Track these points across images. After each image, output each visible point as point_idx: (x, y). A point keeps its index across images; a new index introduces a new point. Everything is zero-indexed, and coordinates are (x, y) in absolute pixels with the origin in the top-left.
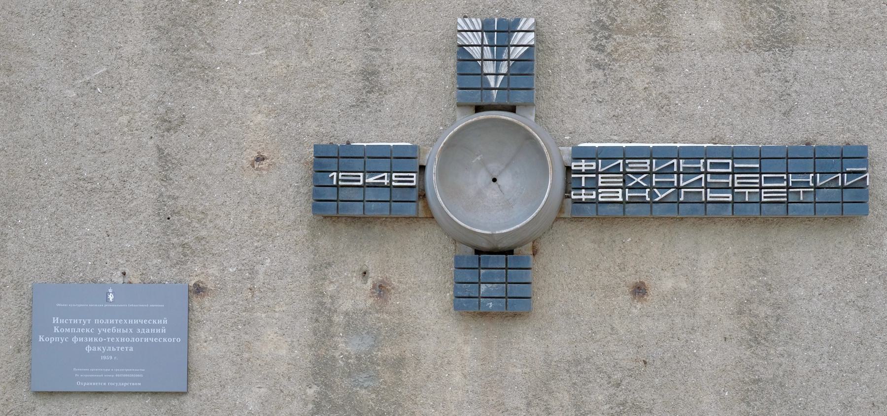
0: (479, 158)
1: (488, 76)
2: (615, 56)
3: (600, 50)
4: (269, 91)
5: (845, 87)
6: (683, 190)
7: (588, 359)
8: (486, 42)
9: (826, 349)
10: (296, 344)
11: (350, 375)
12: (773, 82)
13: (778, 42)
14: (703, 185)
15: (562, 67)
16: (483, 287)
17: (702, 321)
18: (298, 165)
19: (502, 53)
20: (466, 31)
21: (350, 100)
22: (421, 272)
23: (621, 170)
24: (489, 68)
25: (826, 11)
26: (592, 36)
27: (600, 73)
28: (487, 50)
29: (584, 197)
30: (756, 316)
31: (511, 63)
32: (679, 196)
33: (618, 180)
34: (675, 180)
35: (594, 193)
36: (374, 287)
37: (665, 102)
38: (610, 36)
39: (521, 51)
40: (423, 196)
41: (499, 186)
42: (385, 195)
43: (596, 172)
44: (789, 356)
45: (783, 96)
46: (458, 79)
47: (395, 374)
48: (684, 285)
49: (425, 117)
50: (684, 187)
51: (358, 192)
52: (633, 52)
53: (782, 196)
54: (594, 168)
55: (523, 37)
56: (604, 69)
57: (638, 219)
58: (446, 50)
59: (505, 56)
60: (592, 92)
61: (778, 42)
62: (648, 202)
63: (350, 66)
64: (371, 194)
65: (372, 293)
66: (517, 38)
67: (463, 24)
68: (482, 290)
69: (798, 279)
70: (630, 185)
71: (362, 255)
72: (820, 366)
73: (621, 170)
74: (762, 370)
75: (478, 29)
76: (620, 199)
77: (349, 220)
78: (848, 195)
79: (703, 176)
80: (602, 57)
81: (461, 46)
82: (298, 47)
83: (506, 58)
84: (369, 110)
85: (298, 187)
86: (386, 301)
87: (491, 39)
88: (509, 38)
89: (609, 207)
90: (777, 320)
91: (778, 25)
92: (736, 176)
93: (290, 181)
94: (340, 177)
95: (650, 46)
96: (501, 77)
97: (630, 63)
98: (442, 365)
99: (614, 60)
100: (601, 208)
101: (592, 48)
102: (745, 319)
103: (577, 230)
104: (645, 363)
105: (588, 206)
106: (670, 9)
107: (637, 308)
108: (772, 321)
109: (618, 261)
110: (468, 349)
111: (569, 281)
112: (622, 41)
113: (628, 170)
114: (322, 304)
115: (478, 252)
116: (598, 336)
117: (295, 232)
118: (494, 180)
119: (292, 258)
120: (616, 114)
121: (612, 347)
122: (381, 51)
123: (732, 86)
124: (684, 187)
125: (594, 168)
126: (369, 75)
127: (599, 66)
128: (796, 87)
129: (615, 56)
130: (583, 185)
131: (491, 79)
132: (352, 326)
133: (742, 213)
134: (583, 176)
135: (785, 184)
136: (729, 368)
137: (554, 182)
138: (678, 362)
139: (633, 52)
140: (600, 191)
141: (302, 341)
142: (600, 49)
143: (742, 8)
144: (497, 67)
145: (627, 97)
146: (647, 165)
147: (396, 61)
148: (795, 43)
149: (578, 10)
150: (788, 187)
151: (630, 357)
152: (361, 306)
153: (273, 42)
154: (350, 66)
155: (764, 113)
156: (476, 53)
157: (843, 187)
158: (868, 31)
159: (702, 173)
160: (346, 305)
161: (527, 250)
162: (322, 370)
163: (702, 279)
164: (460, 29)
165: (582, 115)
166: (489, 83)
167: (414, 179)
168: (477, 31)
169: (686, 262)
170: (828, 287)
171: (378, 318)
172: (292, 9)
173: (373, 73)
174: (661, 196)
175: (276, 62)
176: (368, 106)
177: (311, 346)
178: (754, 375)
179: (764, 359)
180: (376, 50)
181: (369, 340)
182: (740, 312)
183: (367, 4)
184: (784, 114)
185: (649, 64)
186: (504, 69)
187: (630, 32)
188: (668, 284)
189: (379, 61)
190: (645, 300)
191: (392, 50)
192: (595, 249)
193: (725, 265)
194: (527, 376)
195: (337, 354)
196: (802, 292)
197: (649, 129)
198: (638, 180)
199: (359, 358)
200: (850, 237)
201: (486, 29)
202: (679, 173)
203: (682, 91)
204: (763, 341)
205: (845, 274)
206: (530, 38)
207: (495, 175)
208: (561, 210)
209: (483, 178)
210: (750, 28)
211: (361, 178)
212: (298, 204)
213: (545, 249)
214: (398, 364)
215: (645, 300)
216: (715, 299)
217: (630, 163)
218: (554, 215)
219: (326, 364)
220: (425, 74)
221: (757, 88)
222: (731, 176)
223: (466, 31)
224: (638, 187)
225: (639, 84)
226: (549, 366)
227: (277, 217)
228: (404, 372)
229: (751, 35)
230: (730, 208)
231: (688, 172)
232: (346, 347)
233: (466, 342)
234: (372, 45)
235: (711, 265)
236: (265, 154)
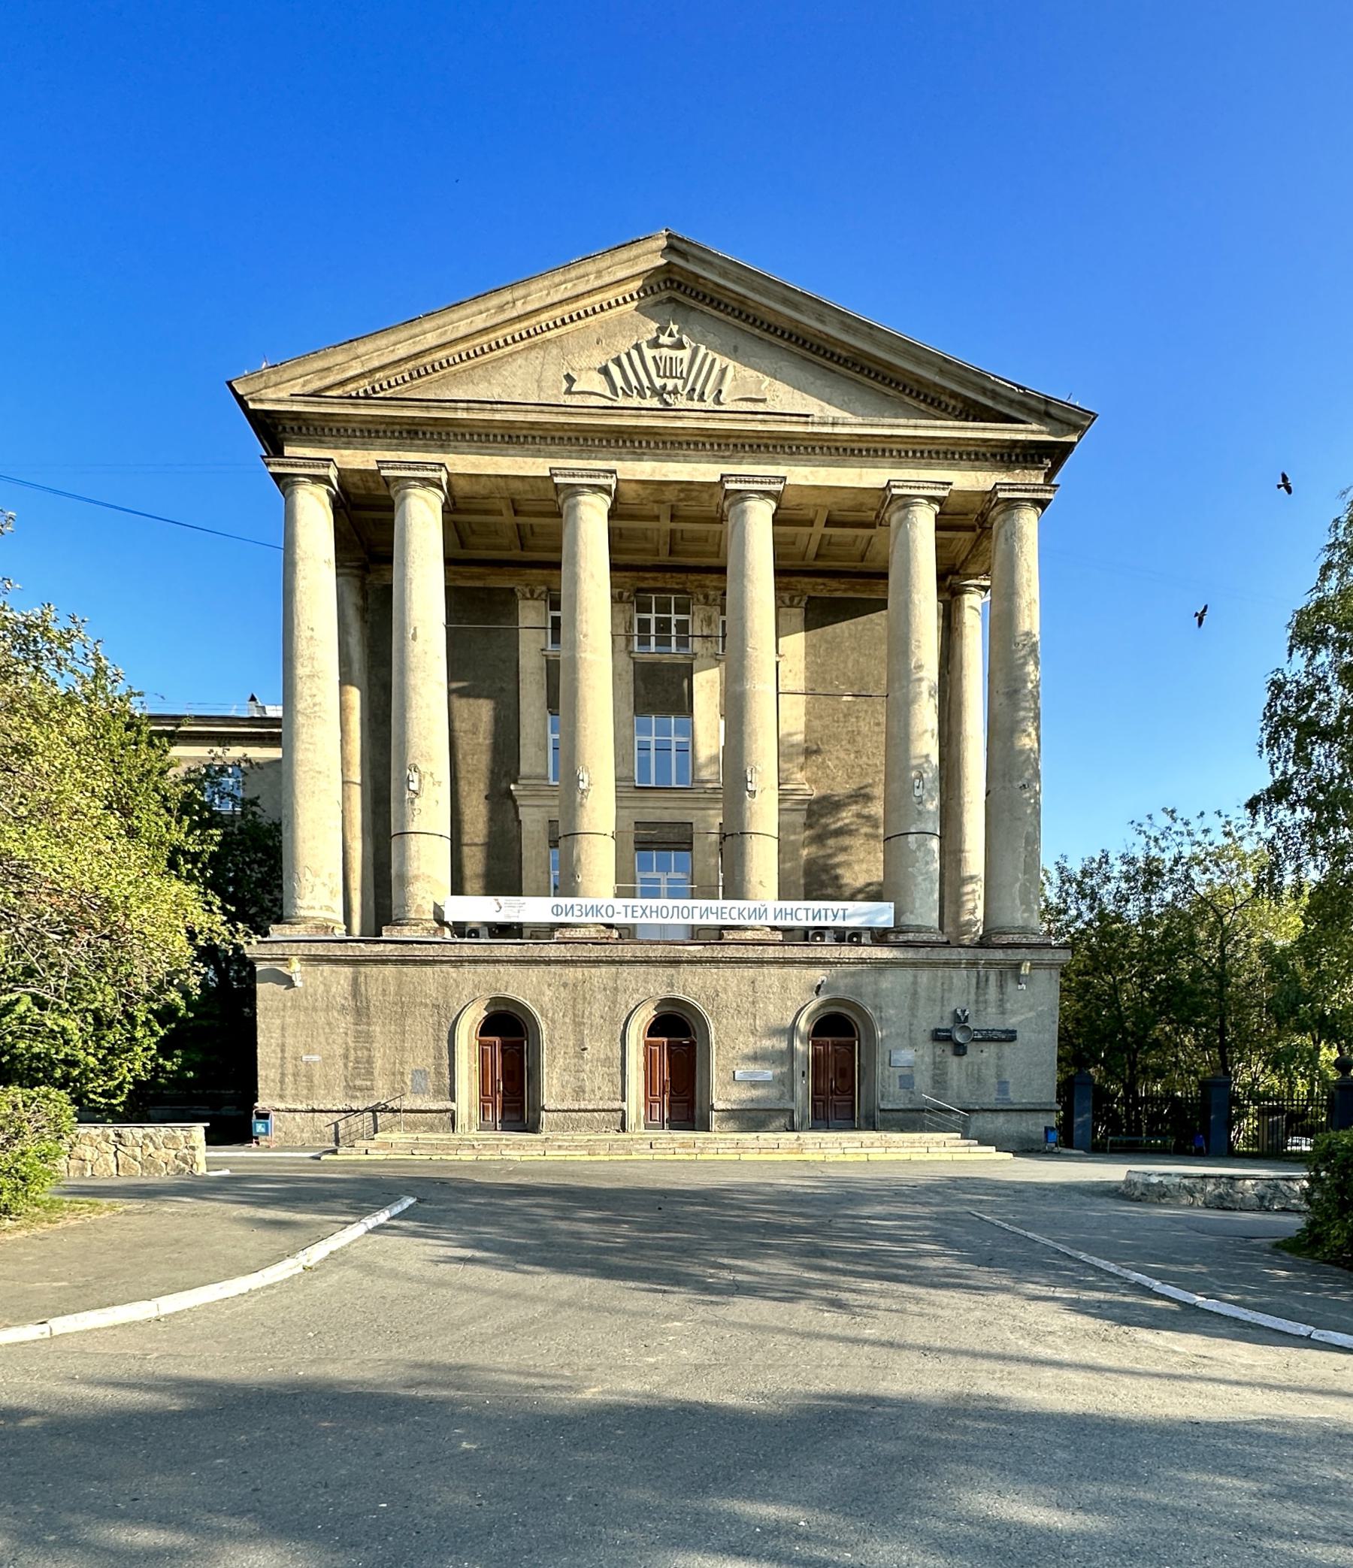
22: (949, 1049)
51: (939, 1037)
93: (927, 1035)
133: (999, 1040)
162: (934, 1063)
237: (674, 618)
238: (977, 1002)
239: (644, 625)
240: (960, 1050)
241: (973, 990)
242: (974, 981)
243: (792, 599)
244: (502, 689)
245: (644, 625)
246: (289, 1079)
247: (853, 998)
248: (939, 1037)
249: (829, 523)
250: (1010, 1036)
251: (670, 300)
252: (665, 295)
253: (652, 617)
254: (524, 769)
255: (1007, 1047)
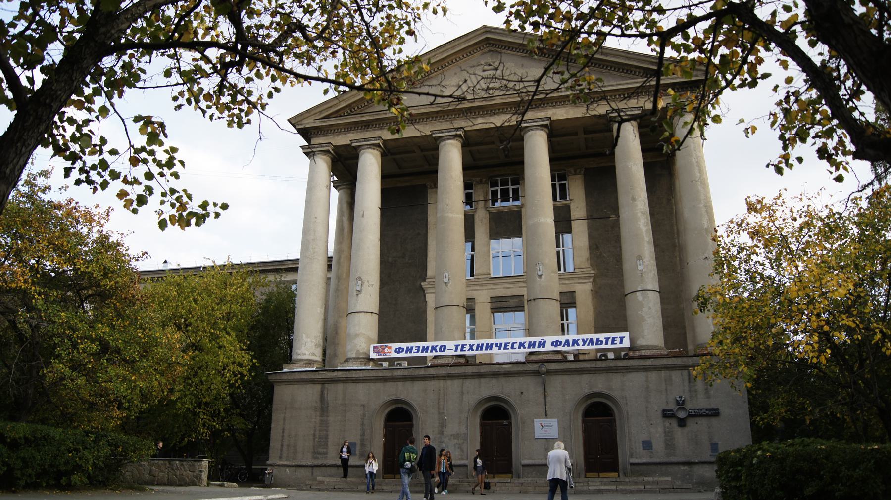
13: (709, 397)
22: (674, 423)
51: (667, 415)
93: (659, 413)
162: (665, 432)
237: (511, 188)
238: (690, 391)
239: (495, 193)
240: (682, 423)
241: (686, 383)
242: (686, 377)
243: (575, 171)
244: (419, 234)
245: (495, 193)
246: (285, 448)
247: (607, 392)
248: (667, 415)
249: (585, 132)
250: (715, 413)
251: (490, 51)
252: (487, 50)
253: (499, 189)
254: (430, 273)
255: (714, 421)
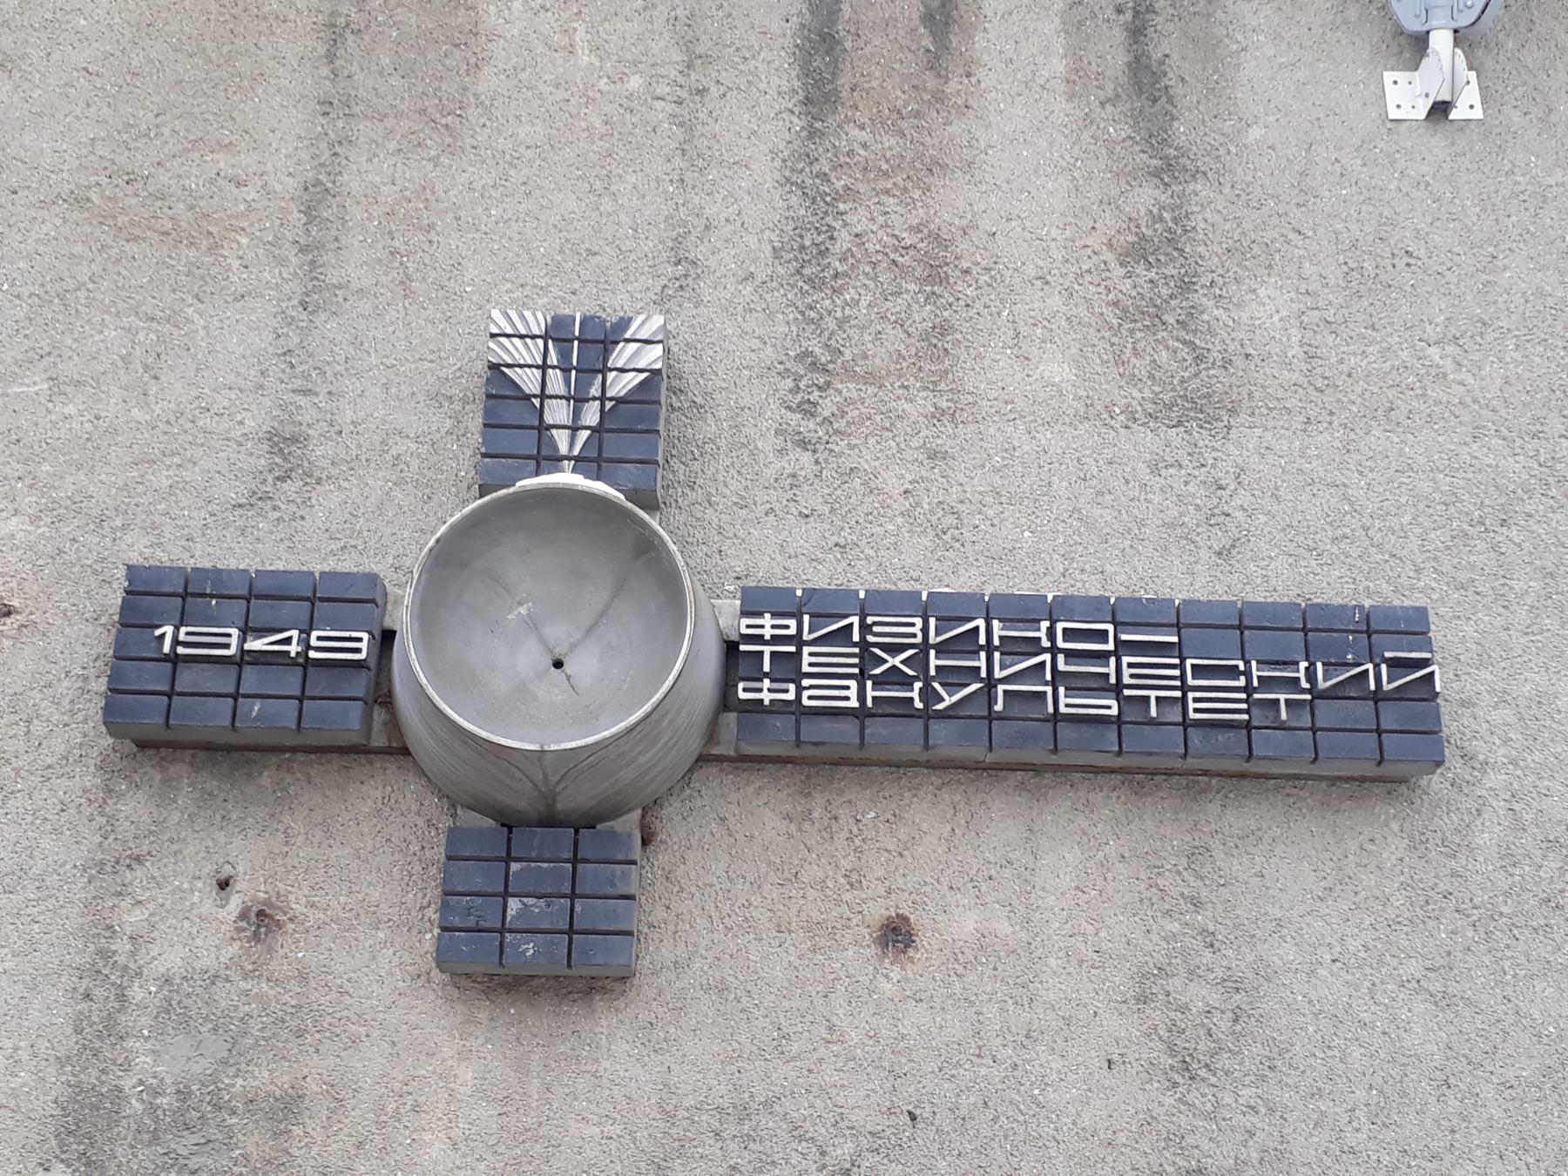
0: (523, 610)
1: (554, 432)
2: (840, 424)
3: (806, 412)
4: (46, 467)
5: (1351, 504)
6: (1001, 688)
7: (767, 1104)
8: (553, 359)
9: (1360, 1094)
10: (24, 1055)
11: (155, 1138)
12: (1190, 488)
13: (1196, 408)
14: (1048, 677)
15: (722, 443)
16: (514, 905)
17: (1051, 1016)
18: (90, 629)
19: (590, 384)
20: (508, 336)
21: (233, 491)
22: (356, 879)
23: (856, 638)
24: (557, 413)
25: (1296, 351)
26: (789, 383)
27: (806, 458)
28: (555, 376)
29: (766, 697)
30: (1184, 1009)
31: (609, 405)
32: (991, 701)
33: (846, 658)
34: (983, 663)
35: (792, 687)
36: (243, 915)
37: (950, 520)
38: (828, 384)
39: (631, 380)
40: (382, 696)
41: (568, 678)
42: (290, 682)
43: (797, 639)
44: (1272, 1111)
45: (1215, 517)
46: (483, 434)
47: (277, 1135)
48: (1004, 928)
49: (406, 534)
50: (1004, 680)
51: (230, 694)
52: (878, 418)
53: (1234, 707)
54: (792, 631)
55: (636, 353)
56: (814, 451)
57: (897, 765)
58: (465, 401)
59: (595, 391)
60: (790, 495)
61: (1196, 408)
62: (916, 714)
63: (241, 423)
64: (252, 679)
65: (239, 930)
66: (622, 355)
67: (503, 323)
68: (510, 913)
69: (1279, 923)
70: (877, 671)
71: (223, 840)
72: (1351, 1139)
73: (856, 638)
74: (1206, 1146)
75: (537, 332)
76: (854, 703)
77: (201, 754)
78: (1391, 716)
79: (1047, 657)
80: (812, 425)
81: (494, 367)
82: (125, 380)
83: (598, 394)
84: (277, 514)
85: (86, 679)
86: (270, 950)
87: (565, 355)
88: (606, 353)
89: (826, 724)
90: (1236, 1021)
91: (1196, 375)
92: (1126, 660)
94: (182, 637)
95: (923, 404)
96: (584, 434)
97: (872, 441)
98: (397, 1115)
99: (836, 432)
100: (810, 730)
101: (789, 408)
102: (1157, 1015)
103: (750, 790)
104: (913, 1117)
105: (777, 722)
106: (959, 336)
107: (892, 977)
108: (1223, 1023)
109: (845, 864)
110: (467, 1074)
111: (726, 909)
112: (854, 395)
113: (871, 639)
114: (105, 954)
115: (509, 823)
116: (795, 1048)
117: (65, 782)
118: (558, 664)
119: (46, 842)
120: (842, 541)
121: (830, 1076)
122: (317, 394)
123: (1100, 493)
124: (1004, 680)
125: (792, 631)
126: (284, 445)
127: (804, 444)
128: (1243, 498)
129: (840, 424)
130: (766, 668)
131: (561, 439)
132: (175, 1011)
134: (767, 650)
135: (1242, 682)
136: (1122, 1138)
137: (692, 661)
138: (995, 1119)
139: (878, 418)
140: (805, 682)
141: (42, 1045)
142: (807, 409)
143: (1114, 340)
144: (577, 414)
145: (865, 508)
146: (917, 630)
147: (349, 415)
148: (1233, 412)
149: (760, 331)
150: (1248, 689)
151: (874, 1099)
152: (207, 961)
153: (68, 369)
154: (241, 423)
155: (1174, 550)
156: (529, 381)
157: (1378, 697)
158: (1391, 393)
159: (1045, 650)
160: (168, 958)
161: (629, 823)
163: (1048, 915)
164: (495, 330)
165: (765, 524)
166: (556, 449)
167: (364, 645)
168: (533, 337)
169: (1007, 873)
170: (1353, 945)
171: (247, 993)
172: (121, 305)
173: (294, 440)
174: (949, 700)
175: (70, 409)
176: (275, 508)
177: (63, 1062)
178: (1187, 1158)
179: (1208, 1117)
180: (307, 392)
181: (216, 1047)
182: (1143, 999)
183: (295, 302)
184: (1219, 554)
185: (915, 444)
186: (591, 415)
187: (870, 378)
188: (966, 924)
189: (308, 416)
190: (911, 959)
191: (342, 395)
192: (790, 836)
193: (1100, 883)
194: (613, 1145)
195: (128, 1083)
196: (1289, 952)
197: (915, 575)
198: (896, 661)
199: (183, 1094)
200: (1395, 826)
201: (557, 333)
202: (989, 649)
203: (989, 500)
204: (1203, 1073)
205: (1391, 913)
206: (652, 356)
207: (559, 652)
208: (712, 735)
209: (531, 658)
210: (1134, 380)
211: (234, 641)
212: (80, 717)
213: (673, 826)
214: (286, 1109)
215: (911, 959)
216: (1081, 962)
217: (875, 624)
218: (694, 745)
219: (95, 1107)
220: (413, 446)
221: (1156, 499)
222: (1113, 660)
223: (508, 336)
224: (894, 677)
225: (892, 482)
226: (669, 1117)
227: (22, 746)
228: (297, 1131)
229: (1136, 393)
230: (1114, 737)
231: (1013, 648)
232: (153, 1064)
233: (464, 1055)
234: (298, 383)
235: (1067, 881)
236: (15, 603)
238: (810, 260)
240: (542, 888)
241: (756, 118)
250: (1323, 712)
255: (1300, 896)
